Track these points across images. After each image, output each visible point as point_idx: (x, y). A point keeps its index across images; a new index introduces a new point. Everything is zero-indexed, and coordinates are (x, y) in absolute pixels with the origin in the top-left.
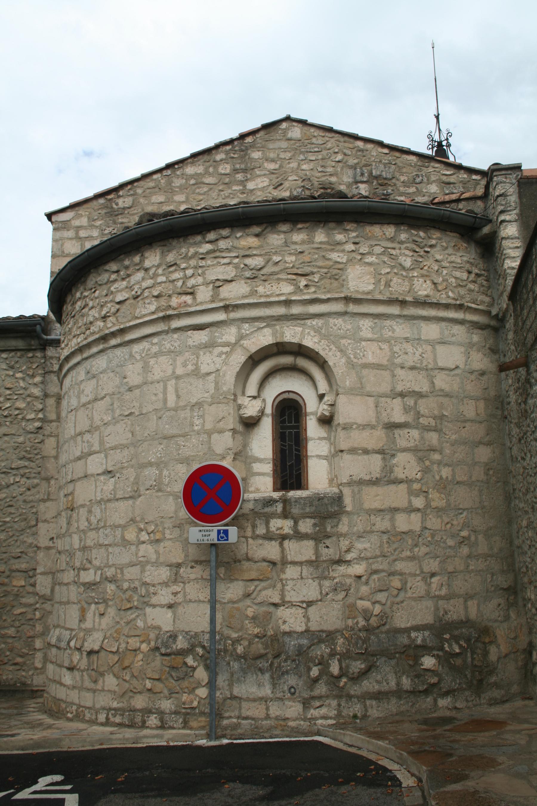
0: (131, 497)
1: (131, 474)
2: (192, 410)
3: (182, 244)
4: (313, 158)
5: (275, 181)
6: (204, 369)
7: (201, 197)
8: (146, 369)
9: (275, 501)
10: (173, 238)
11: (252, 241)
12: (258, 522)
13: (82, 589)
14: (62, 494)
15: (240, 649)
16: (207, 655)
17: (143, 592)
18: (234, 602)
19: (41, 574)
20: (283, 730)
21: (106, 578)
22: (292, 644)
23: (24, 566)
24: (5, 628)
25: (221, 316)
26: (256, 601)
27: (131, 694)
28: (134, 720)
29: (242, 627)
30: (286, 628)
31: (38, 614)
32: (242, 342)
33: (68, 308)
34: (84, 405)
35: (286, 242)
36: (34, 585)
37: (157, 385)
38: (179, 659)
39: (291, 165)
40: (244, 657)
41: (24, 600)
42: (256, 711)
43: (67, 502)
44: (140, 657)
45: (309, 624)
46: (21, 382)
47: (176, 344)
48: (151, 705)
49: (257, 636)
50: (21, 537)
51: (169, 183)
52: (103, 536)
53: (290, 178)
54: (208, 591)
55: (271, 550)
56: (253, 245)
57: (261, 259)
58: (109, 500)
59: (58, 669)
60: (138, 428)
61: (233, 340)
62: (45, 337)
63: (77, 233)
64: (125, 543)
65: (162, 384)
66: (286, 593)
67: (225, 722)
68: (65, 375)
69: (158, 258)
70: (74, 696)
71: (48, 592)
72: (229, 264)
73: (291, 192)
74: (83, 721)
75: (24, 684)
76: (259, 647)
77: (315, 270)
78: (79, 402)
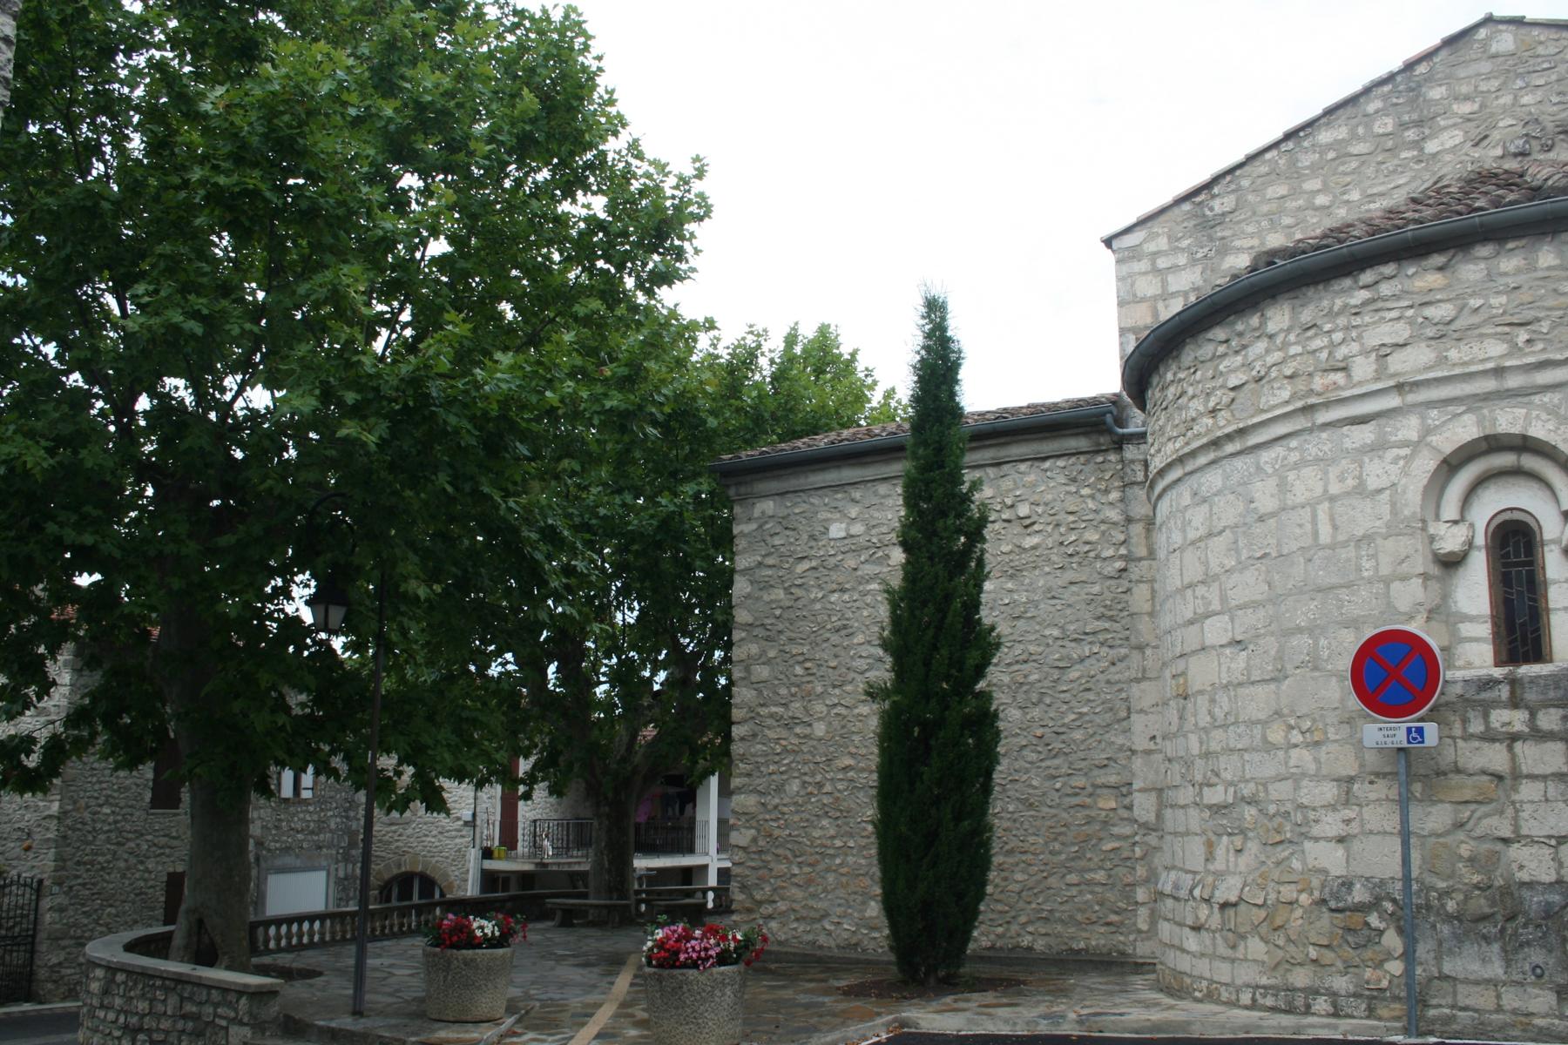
0: (1272, 679)
1: (1271, 644)
2: (1358, 547)
3: (1323, 294)
4: (1542, 82)
5: (1475, 133)
6: (1372, 483)
7: (1348, 179)
8: (1283, 487)
9: (1497, 682)
10: (1308, 285)
11: (1433, 279)
12: (1471, 714)
13: (1207, 813)
14: (1168, 674)
15: (1451, 906)
16: (1400, 913)
17: (1299, 819)
18: (1439, 836)
19: (1140, 790)
20: (1524, 1030)
21: (1243, 798)
22: (1534, 900)
23: (1113, 779)
24: (1091, 870)
25: (1393, 401)
26: (1474, 834)
27: (1287, 966)
28: (1293, 1002)
29: (1453, 871)
30: (1524, 876)
31: (1138, 851)
32: (1429, 439)
33: (1153, 394)
34: (1193, 543)
35: (1489, 275)
36: (1129, 808)
37: (1302, 512)
38: (1358, 917)
39: (1501, 101)
40: (1458, 917)
41: (1115, 830)
42: (1482, 999)
43: (1178, 686)
44: (1299, 912)
45: (1563, 872)
46: (1089, 501)
47: (1325, 448)
48: (1318, 983)
49: (1476, 886)
50: (1107, 736)
51: (1293, 163)
52: (1233, 738)
53: (1501, 124)
54: (1397, 818)
55: (1495, 757)
56: (1436, 285)
57: (1449, 306)
58: (1240, 684)
59: (1177, 929)
60: (1277, 577)
61: (1414, 436)
62: (1120, 431)
63: (1154, 263)
64: (1269, 747)
65: (1308, 509)
66: (1522, 823)
67: (1432, 1013)
68: (1160, 496)
69: (1287, 317)
70: (1203, 967)
71: (1152, 818)
72: (1399, 318)
73: (1504, 147)
74: (1218, 1002)
75: (1123, 953)
76: (1480, 904)
77: (1542, 315)
78: (1185, 538)
